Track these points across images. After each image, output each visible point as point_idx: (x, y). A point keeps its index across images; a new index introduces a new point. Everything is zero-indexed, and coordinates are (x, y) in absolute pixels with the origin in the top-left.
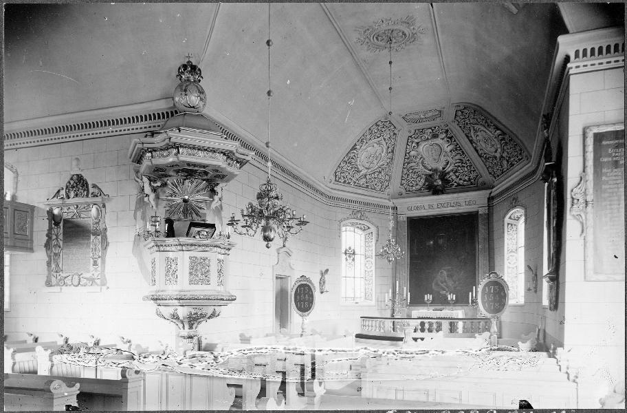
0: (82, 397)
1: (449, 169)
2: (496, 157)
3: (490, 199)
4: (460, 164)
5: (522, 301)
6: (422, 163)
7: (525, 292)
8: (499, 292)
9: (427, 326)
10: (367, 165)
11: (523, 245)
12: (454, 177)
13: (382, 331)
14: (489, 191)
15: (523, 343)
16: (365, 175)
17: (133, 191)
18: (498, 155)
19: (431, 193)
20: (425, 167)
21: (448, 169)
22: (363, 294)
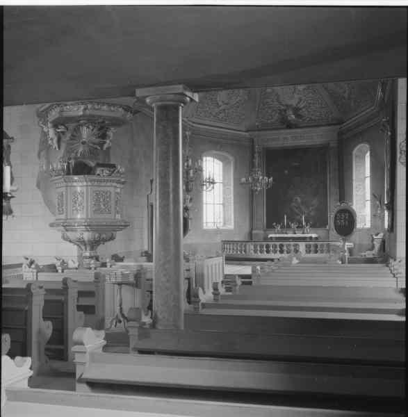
0: (27, 311)
1: (302, 106)
2: (344, 98)
3: (340, 134)
4: (312, 102)
5: (368, 225)
6: (278, 100)
7: (371, 218)
8: (346, 224)
9: (285, 248)
10: (226, 101)
11: (369, 199)
12: (306, 113)
13: (235, 252)
14: (339, 127)
15: (31, 377)
16: (224, 110)
17: (37, 136)
18: (346, 95)
19: (285, 126)
20: (280, 103)
21: (301, 105)
22: (222, 220)
